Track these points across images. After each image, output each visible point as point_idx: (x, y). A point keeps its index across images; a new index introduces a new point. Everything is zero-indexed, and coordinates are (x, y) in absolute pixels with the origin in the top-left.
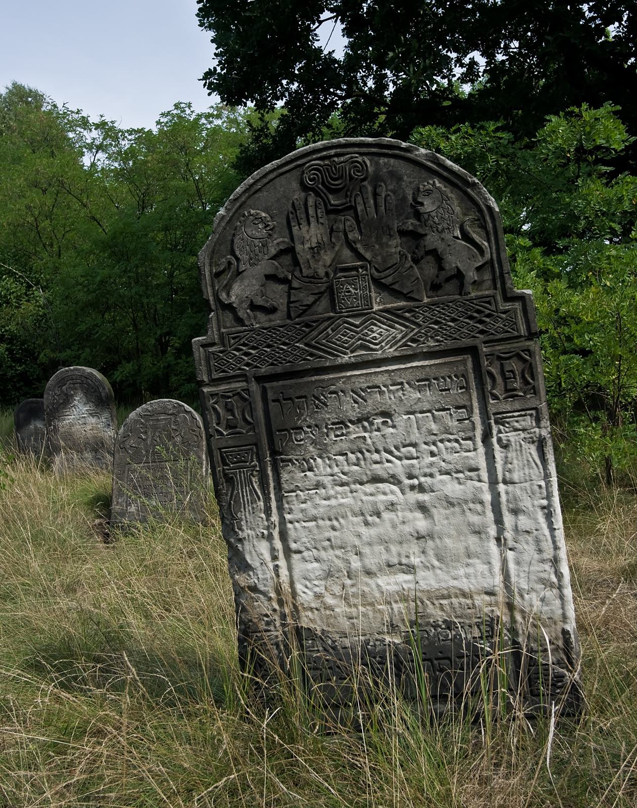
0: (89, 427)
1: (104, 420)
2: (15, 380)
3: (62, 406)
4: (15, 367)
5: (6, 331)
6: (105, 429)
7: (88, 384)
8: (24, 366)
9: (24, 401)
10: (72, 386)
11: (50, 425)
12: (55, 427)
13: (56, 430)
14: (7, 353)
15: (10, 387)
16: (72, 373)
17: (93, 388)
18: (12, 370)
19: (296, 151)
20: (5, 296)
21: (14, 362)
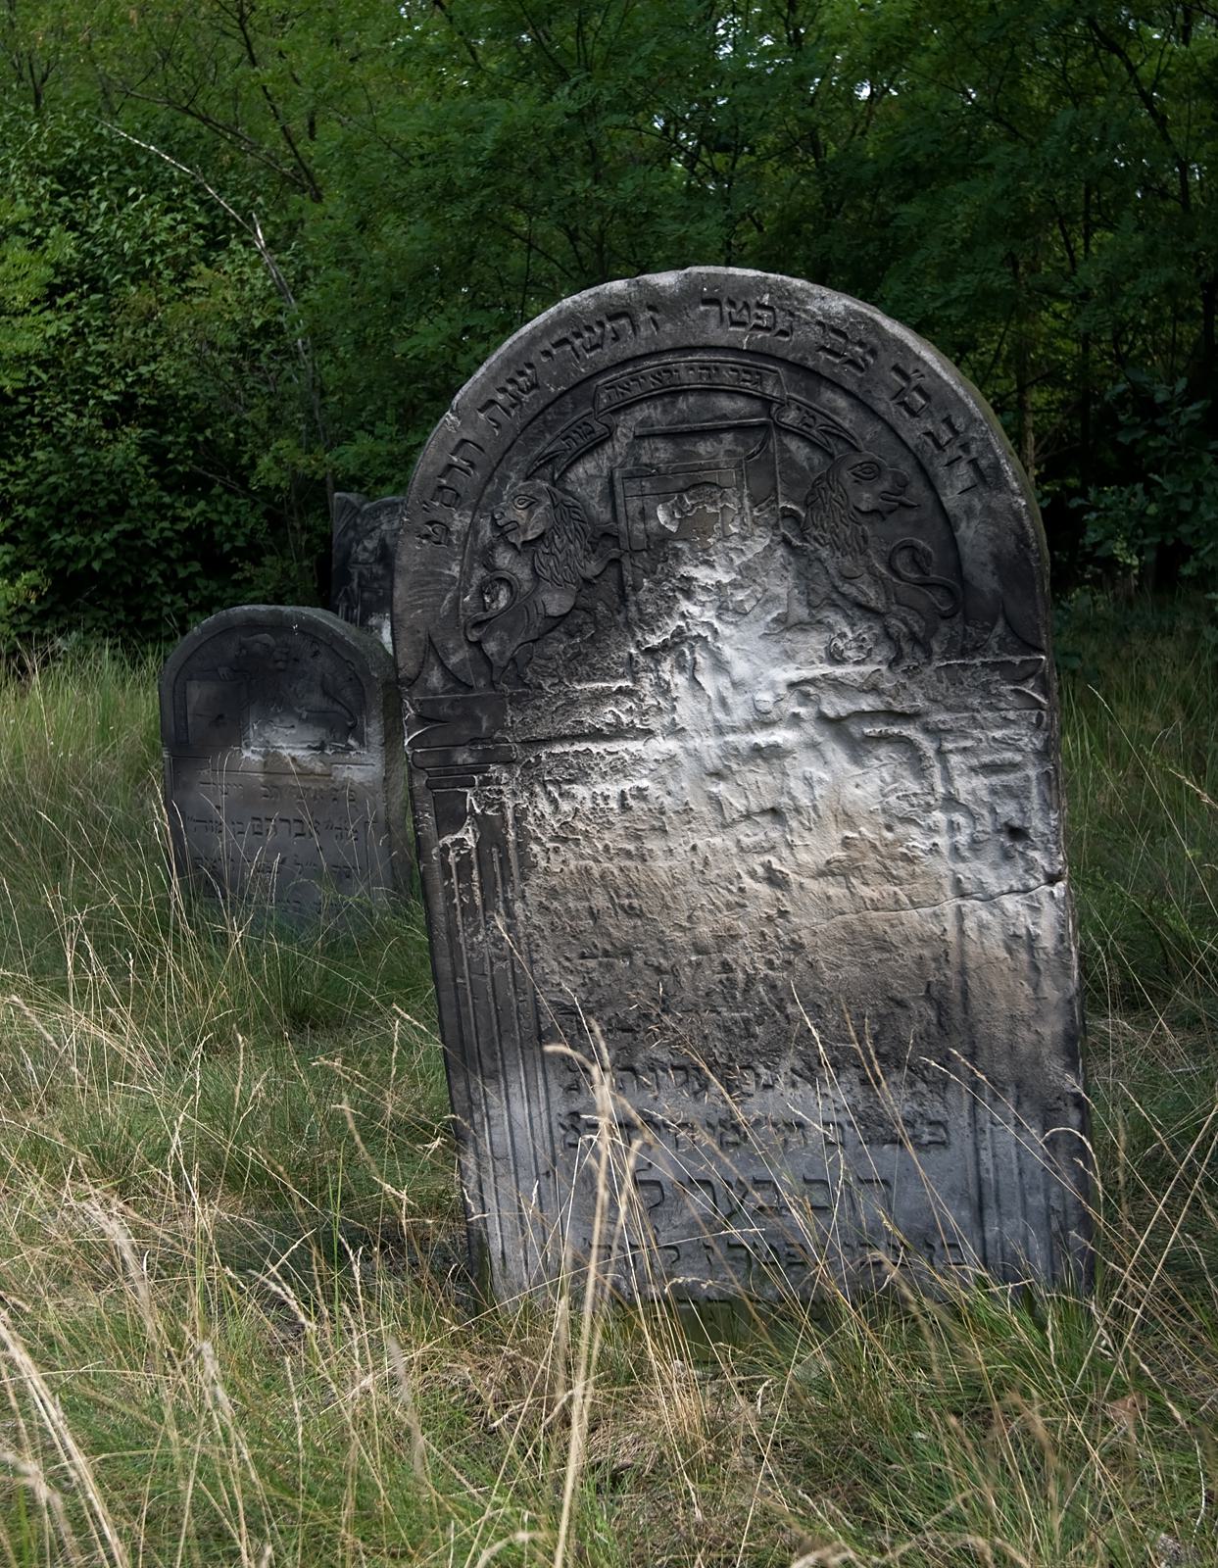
0: (817, 848)
1: (966, 786)
2: (173, 554)
3: (558, 645)
4: (171, 506)
5: (140, 380)
6: (983, 872)
7: (829, 439)
8: (201, 505)
9: (201, 625)
10: (662, 452)
11: (451, 819)
12: (491, 832)
13: (501, 858)
14: (144, 459)
15: (155, 577)
16: (670, 332)
17: (871, 472)
18: (164, 518)
19: (529, 326)
20: (137, 258)
21: (170, 490)
